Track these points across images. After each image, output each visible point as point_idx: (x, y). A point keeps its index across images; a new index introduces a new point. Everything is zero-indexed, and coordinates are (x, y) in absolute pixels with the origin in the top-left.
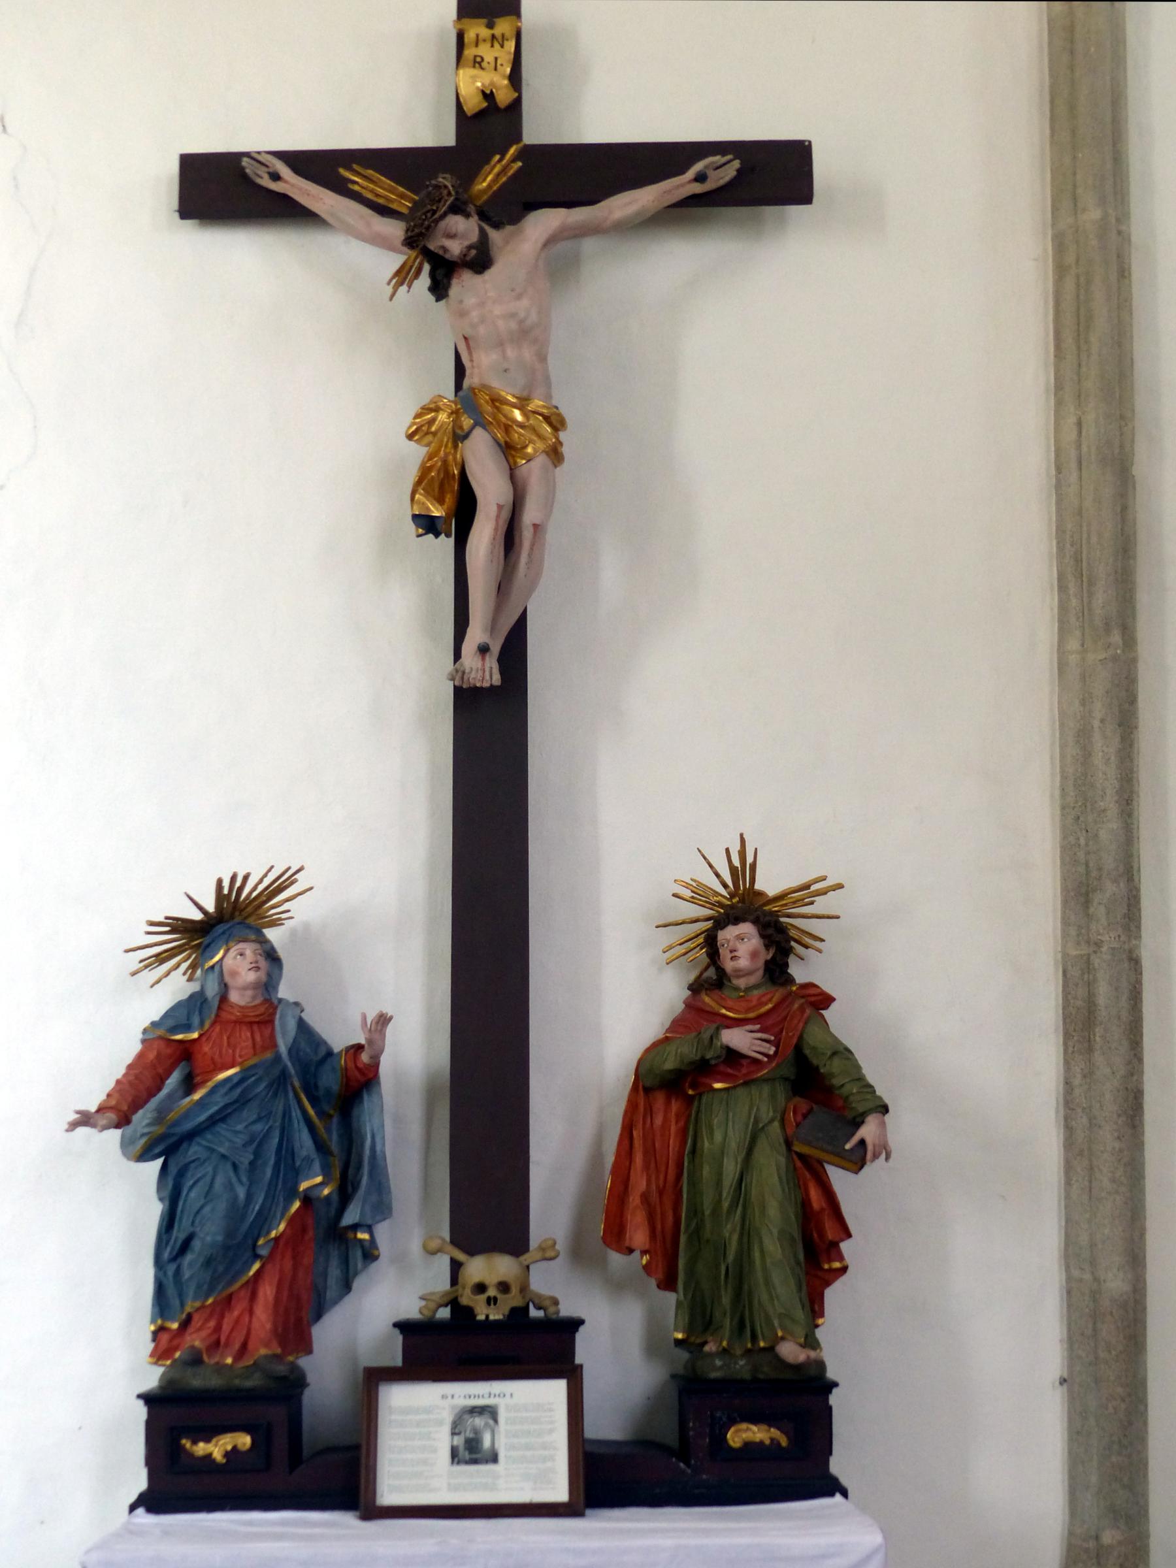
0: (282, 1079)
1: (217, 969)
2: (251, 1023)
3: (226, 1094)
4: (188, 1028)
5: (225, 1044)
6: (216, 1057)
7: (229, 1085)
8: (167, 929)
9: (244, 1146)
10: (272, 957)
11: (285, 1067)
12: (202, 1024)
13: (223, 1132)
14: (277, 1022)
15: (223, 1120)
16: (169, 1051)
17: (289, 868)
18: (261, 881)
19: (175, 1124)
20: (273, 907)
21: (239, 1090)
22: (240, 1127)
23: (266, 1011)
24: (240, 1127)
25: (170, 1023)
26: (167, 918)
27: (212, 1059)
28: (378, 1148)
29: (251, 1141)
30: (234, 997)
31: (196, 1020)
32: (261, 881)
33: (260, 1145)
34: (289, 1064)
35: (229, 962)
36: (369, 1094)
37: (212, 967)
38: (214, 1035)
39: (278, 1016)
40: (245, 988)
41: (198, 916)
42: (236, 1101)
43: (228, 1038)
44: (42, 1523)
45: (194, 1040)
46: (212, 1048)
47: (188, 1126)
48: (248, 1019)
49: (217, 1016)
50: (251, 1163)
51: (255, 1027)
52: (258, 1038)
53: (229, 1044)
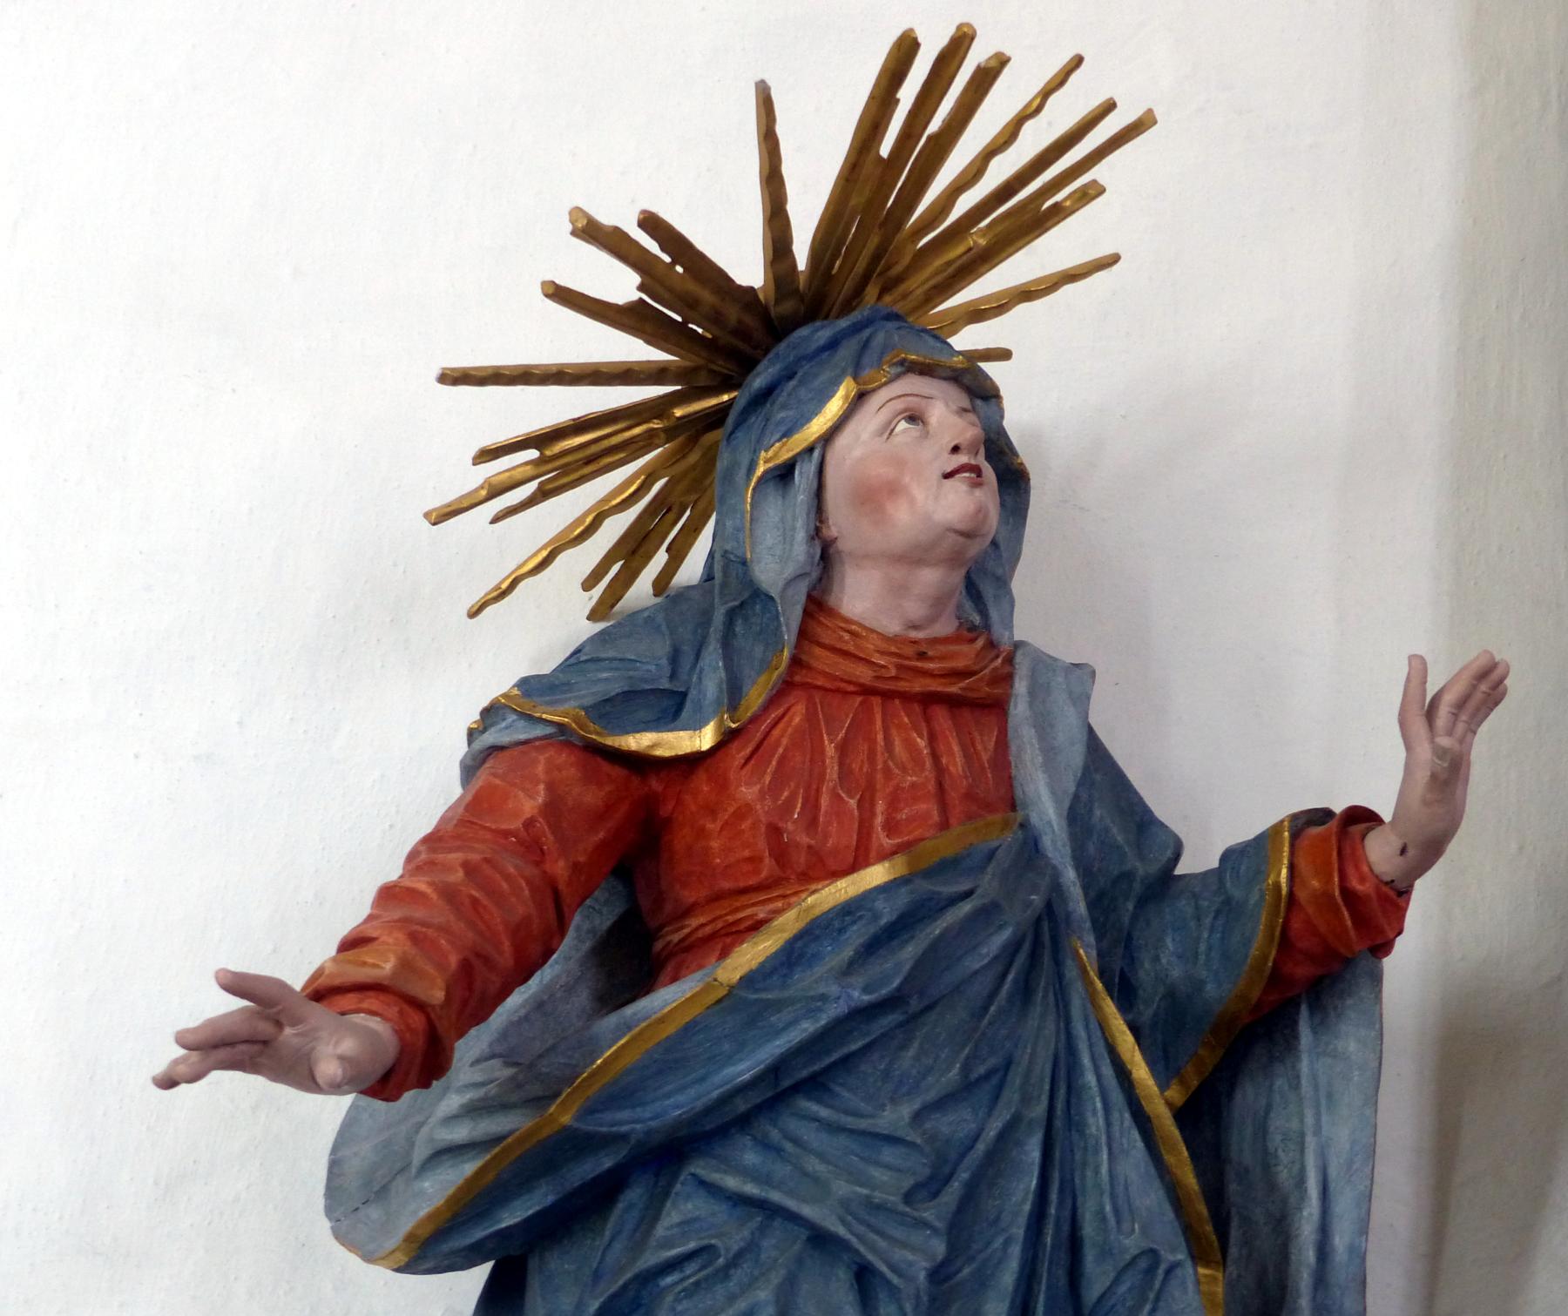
0: (1044, 936)
1: (803, 477)
2: (928, 700)
3: (850, 968)
4: (672, 708)
5: (832, 771)
6: (792, 828)
7: (857, 935)
8: (531, 487)
9: (908, 1198)
10: (1003, 469)
11: (1057, 887)
12: (734, 693)
13: (807, 1132)
14: (1019, 709)
15: (816, 1085)
16: (592, 797)
17: (1109, 107)
18: (1030, 112)
19: (623, 1093)
20: (977, 313)
21: (909, 952)
22: (895, 1117)
23: (967, 680)
24: (895, 1117)
25: (608, 683)
26: (651, 223)
27: (775, 831)
28: (1340, 1242)
29: (932, 1186)
30: (862, 597)
31: (711, 682)
32: (1030, 112)
33: (969, 1197)
34: (1070, 875)
35: (860, 448)
36: (1322, 1024)
37: (784, 474)
38: (782, 738)
39: (1021, 686)
40: (913, 557)
41: (746, 266)
42: (893, 1002)
43: (843, 749)
44: (136, 757)
45: (694, 761)
46: (774, 789)
47: (676, 1103)
48: (918, 686)
49: (796, 662)
50: (939, 1274)
51: (942, 717)
52: (956, 763)
53: (845, 774)
